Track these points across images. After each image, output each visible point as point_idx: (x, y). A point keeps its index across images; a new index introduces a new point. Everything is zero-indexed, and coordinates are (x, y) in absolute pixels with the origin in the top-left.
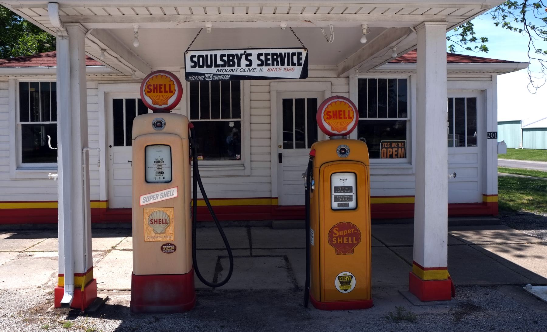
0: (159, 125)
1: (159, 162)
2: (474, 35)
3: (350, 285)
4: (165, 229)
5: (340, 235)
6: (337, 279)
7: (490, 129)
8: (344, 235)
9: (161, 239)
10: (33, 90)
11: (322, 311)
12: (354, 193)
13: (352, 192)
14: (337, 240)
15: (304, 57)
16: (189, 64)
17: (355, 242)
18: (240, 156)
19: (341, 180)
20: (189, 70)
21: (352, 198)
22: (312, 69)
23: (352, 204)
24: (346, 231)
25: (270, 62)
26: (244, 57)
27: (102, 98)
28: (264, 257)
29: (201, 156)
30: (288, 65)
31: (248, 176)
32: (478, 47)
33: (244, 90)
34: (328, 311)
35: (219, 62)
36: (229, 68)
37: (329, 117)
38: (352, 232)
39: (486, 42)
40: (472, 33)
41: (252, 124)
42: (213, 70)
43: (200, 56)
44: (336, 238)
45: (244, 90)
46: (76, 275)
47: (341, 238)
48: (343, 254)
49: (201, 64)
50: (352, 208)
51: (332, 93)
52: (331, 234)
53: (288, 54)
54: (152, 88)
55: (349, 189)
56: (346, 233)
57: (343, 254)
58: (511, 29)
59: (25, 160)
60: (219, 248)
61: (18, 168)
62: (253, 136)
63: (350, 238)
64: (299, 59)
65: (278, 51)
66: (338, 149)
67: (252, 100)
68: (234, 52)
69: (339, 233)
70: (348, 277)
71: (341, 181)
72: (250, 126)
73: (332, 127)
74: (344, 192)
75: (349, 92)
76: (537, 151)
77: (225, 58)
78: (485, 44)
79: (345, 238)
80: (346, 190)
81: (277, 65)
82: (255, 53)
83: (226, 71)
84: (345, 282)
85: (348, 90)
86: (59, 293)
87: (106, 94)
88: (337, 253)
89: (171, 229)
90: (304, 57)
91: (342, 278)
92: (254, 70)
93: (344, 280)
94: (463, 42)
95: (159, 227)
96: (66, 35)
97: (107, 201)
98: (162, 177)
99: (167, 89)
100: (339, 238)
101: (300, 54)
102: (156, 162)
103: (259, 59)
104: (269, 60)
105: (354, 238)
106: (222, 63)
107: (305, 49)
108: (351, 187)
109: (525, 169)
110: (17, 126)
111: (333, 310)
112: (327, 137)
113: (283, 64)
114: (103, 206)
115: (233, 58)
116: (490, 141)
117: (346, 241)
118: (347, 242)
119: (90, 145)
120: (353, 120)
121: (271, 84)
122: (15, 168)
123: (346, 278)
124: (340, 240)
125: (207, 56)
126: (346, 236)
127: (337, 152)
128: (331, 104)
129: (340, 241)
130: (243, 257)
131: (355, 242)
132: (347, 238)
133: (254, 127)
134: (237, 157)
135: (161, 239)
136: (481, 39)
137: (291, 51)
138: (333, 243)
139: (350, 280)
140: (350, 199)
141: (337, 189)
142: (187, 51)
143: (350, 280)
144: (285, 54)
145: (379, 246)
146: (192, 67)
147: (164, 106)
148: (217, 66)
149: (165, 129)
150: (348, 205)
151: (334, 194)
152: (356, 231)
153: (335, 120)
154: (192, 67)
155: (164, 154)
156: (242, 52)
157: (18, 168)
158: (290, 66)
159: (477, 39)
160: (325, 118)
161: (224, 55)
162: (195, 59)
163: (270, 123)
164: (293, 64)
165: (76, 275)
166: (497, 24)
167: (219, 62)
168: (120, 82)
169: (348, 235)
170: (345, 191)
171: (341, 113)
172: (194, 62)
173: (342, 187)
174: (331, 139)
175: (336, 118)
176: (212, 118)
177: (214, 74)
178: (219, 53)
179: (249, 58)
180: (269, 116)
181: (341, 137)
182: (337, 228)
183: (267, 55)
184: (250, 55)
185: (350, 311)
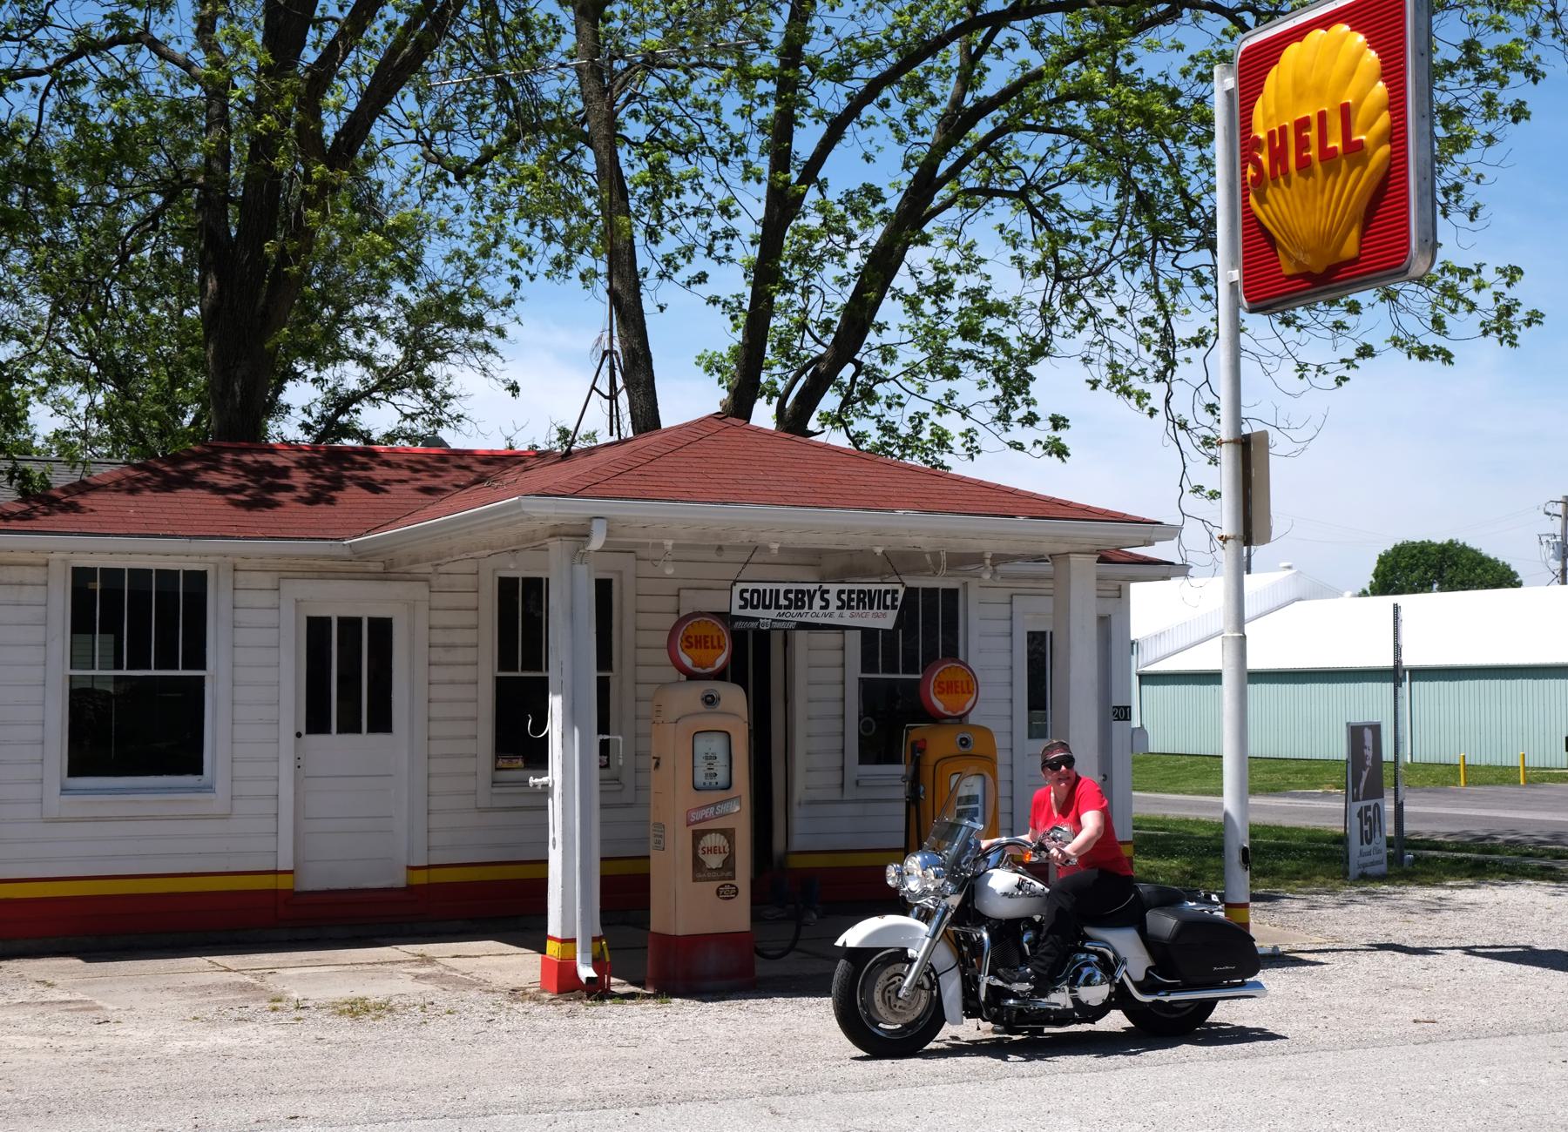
1: (710, 758)
2: (1032, 408)
7: (1116, 703)
16: (737, 602)
25: (854, 604)
26: (818, 594)
30: (879, 608)
32: (1040, 442)
35: (783, 602)
39: (1064, 430)
40: (1028, 402)
42: (773, 613)
43: (754, 591)
54: (693, 640)
58: (1129, 397)
61: (64, 790)
64: (894, 599)
68: (804, 587)
76: (1188, 760)
77: (792, 596)
78: (1061, 433)
83: (791, 615)
92: (831, 615)
94: (1000, 424)
98: (714, 781)
99: (716, 643)
101: (896, 592)
102: (706, 758)
103: (839, 598)
106: (787, 603)
109: (1160, 817)
113: (871, 607)
115: (803, 596)
116: (1117, 725)
121: (683, 593)
136: (1051, 420)
142: (735, 582)
146: (741, 607)
147: (710, 670)
148: (778, 607)
149: (719, 707)
154: (741, 607)
156: (816, 586)
158: (882, 610)
159: (1038, 419)
162: (747, 595)
164: (886, 607)
166: (1095, 384)
167: (783, 602)
168: (333, 575)
178: (783, 587)
179: (826, 596)
183: (851, 592)
184: (827, 592)
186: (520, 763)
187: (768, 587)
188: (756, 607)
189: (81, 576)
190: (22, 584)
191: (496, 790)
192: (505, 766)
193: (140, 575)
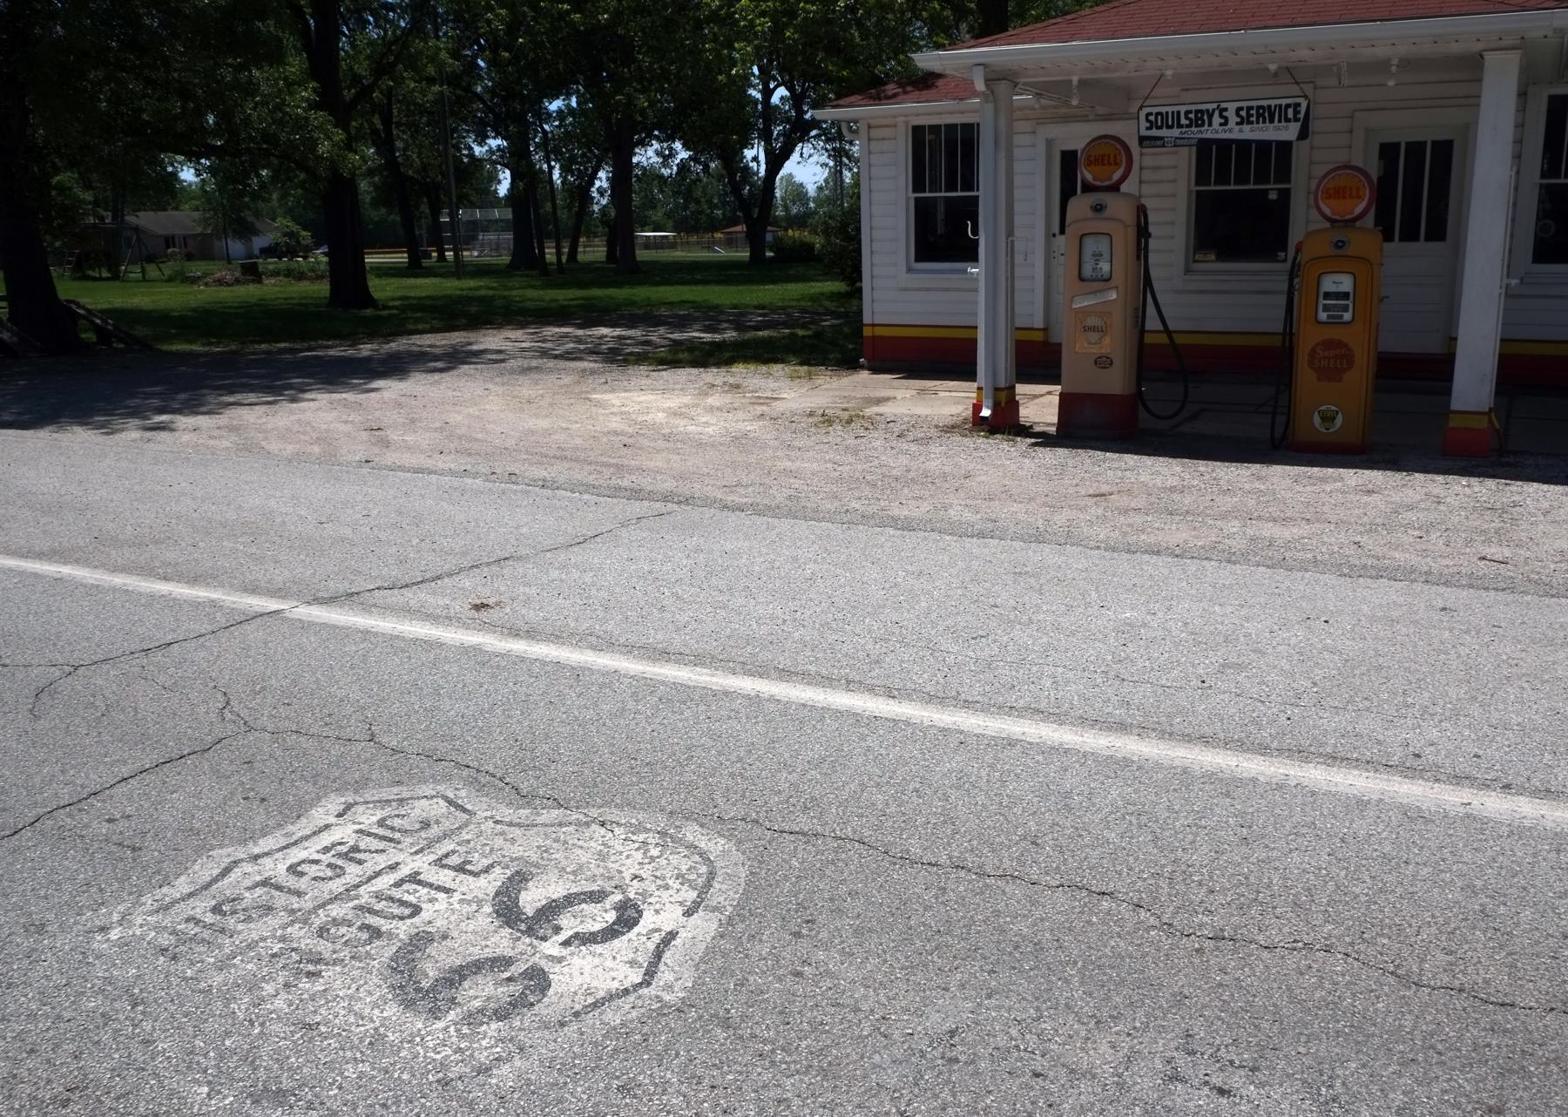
0: (1098, 208)
4: (1100, 339)
6: (1316, 414)
9: (1094, 351)
10: (932, 137)
13: (1348, 299)
15: (1303, 109)
16: (1144, 124)
17: (1345, 366)
20: (1144, 132)
23: (1347, 316)
26: (1217, 113)
27: (1041, 149)
30: (1280, 121)
35: (1184, 121)
36: (1196, 129)
43: (1157, 114)
46: (996, 389)
49: (1159, 123)
52: (1313, 353)
53: (1280, 106)
54: (1092, 159)
55: (1345, 295)
59: (919, 259)
61: (909, 270)
64: (1296, 112)
65: (1265, 103)
74: (1337, 299)
77: (1192, 116)
81: (1264, 122)
82: (1232, 107)
83: (1193, 133)
84: (1328, 419)
86: (977, 408)
87: (1049, 143)
88: (1319, 379)
89: (1107, 340)
90: (1303, 109)
92: (1231, 131)
95: (1094, 336)
96: (991, 98)
97: (1045, 330)
101: (1299, 105)
103: (1238, 114)
104: (1252, 115)
106: (1188, 122)
107: (1306, 97)
110: (908, 199)
112: (1328, 225)
113: (1272, 121)
114: (1039, 337)
115: (1203, 115)
119: (1016, 233)
121: (1356, 114)
122: (904, 269)
125: (1167, 113)
131: (1345, 366)
135: (1096, 350)
137: (1284, 102)
140: (1346, 308)
141: (1327, 295)
142: (1141, 108)
144: (1276, 106)
146: (1147, 129)
147: (1107, 183)
148: (1180, 126)
149: (1107, 213)
150: (1341, 317)
151: (1322, 302)
154: (1147, 129)
155: (1103, 245)
156: (1215, 106)
157: (909, 270)
158: (1283, 124)
161: (1190, 112)
164: (1287, 120)
165: (996, 389)
167: (1184, 121)
172: (1151, 122)
174: (1332, 227)
177: (1176, 138)
178: (1183, 109)
179: (1224, 114)
183: (1249, 109)
184: (1226, 110)
186: (1213, 257)
187: (1170, 109)
188: (1161, 128)
189: (918, 131)
190: (883, 139)
191: (1186, 277)
193: (951, 128)
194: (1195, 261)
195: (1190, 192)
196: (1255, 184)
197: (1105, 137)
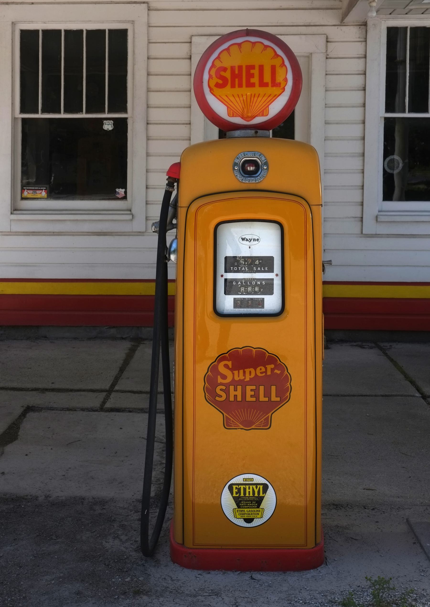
3: (260, 507)
5: (236, 378)
8: (247, 379)
11: (186, 570)
12: (277, 275)
13: (271, 270)
14: (227, 392)
17: (274, 398)
18: (126, 192)
19: (243, 239)
21: (273, 284)
22: (284, 7)
24: (252, 370)
28: (130, 412)
29: (42, 190)
31: (139, 234)
33: (134, 51)
34: (200, 572)
37: (220, 82)
38: (269, 373)
41: (151, 124)
44: (224, 388)
45: (134, 51)
47: (239, 388)
48: (242, 427)
50: (272, 312)
51: (327, 58)
54: (228, 75)
56: (253, 375)
57: (242, 427)
60: (40, 386)
62: (152, 150)
63: (262, 388)
66: (237, 161)
67: (152, 75)
69: (233, 374)
70: (254, 487)
71: (245, 242)
72: (147, 130)
73: (228, 107)
74: (251, 271)
75: (365, 57)
79: (249, 388)
80: (257, 266)
85: (364, 53)
88: (227, 425)
91: (239, 490)
93: (245, 493)
99: (267, 78)
100: (232, 388)
105: (273, 388)
108: (271, 259)
111: (214, 568)
117: (252, 396)
118: (254, 399)
120: (284, 89)
121: (194, 39)
123: (249, 488)
124: (236, 393)
126: (250, 382)
127: (234, 169)
128: (228, 49)
129: (236, 396)
130: (83, 410)
131: (274, 398)
132: (254, 387)
133: (154, 130)
134: (118, 193)
138: (217, 398)
139: (261, 495)
143: (261, 495)
145: (405, 396)
150: (261, 303)
152: (278, 372)
153: (237, 91)
160: (212, 85)
163: (190, 124)
169: (255, 381)
170: (255, 269)
171: (252, 71)
173: (245, 258)
175: (240, 86)
176: (66, 111)
180: (187, 108)
181: (251, 132)
182: (229, 361)
185: (257, 576)
191: (14, 217)
192: (29, 196)
194: (23, 199)
195: (14, 119)
196: (87, 112)
197: (249, 33)
